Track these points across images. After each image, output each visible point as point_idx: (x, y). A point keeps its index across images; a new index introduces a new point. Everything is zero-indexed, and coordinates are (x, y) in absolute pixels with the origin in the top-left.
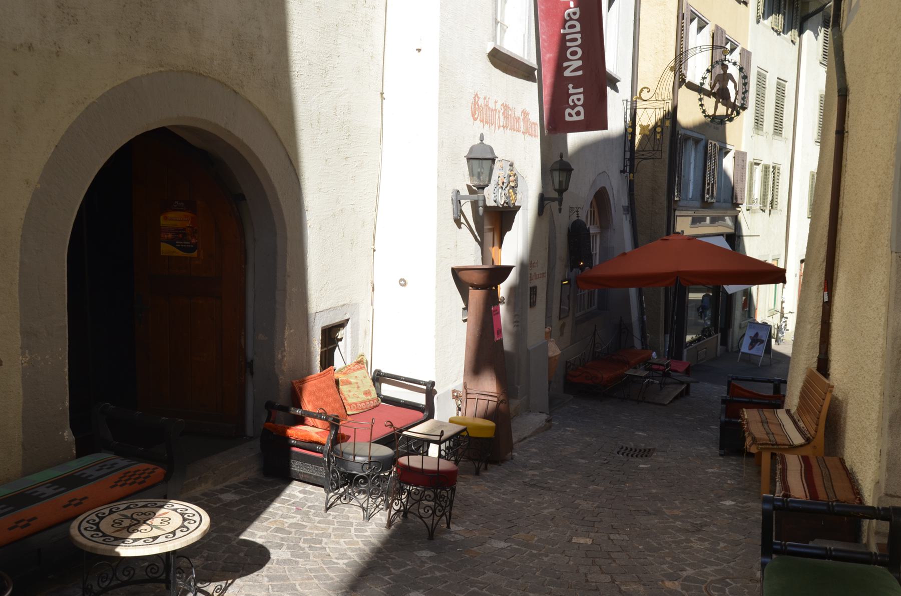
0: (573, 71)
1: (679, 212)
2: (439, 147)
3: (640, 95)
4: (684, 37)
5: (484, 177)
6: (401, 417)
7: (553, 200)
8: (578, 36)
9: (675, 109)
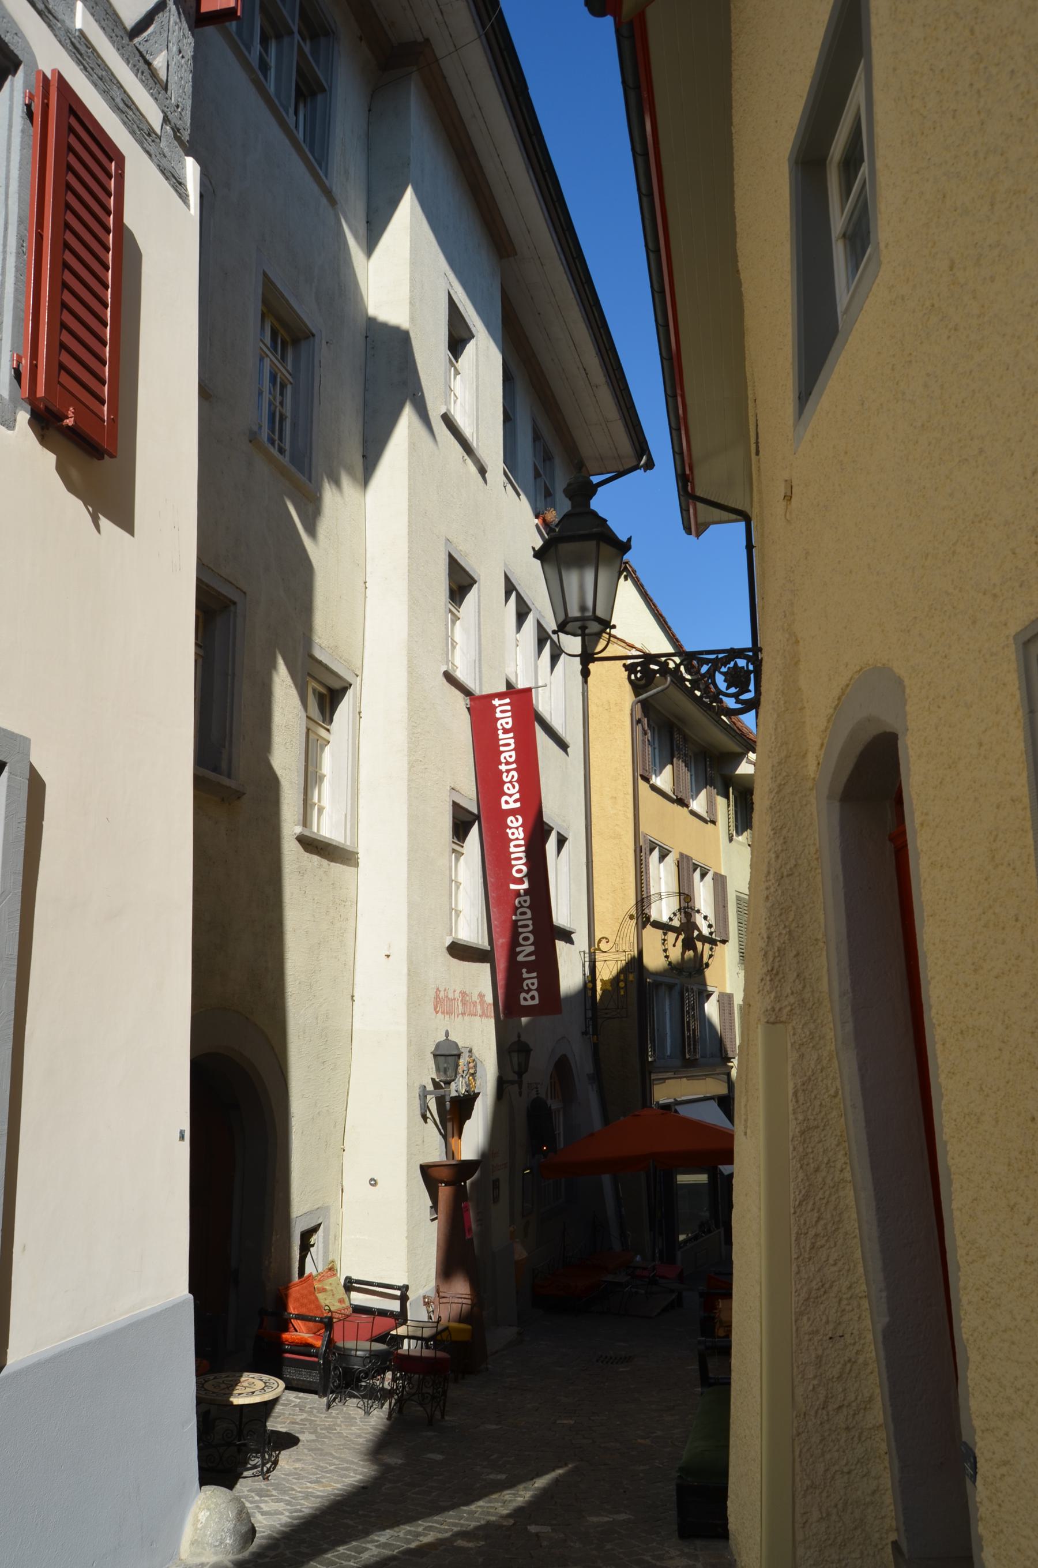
0: (526, 956)
1: (655, 1075)
2: (408, 1046)
3: (598, 946)
4: (644, 872)
5: (450, 1073)
6: (382, 1325)
7: (512, 1082)
8: (530, 922)
9: (640, 953)
